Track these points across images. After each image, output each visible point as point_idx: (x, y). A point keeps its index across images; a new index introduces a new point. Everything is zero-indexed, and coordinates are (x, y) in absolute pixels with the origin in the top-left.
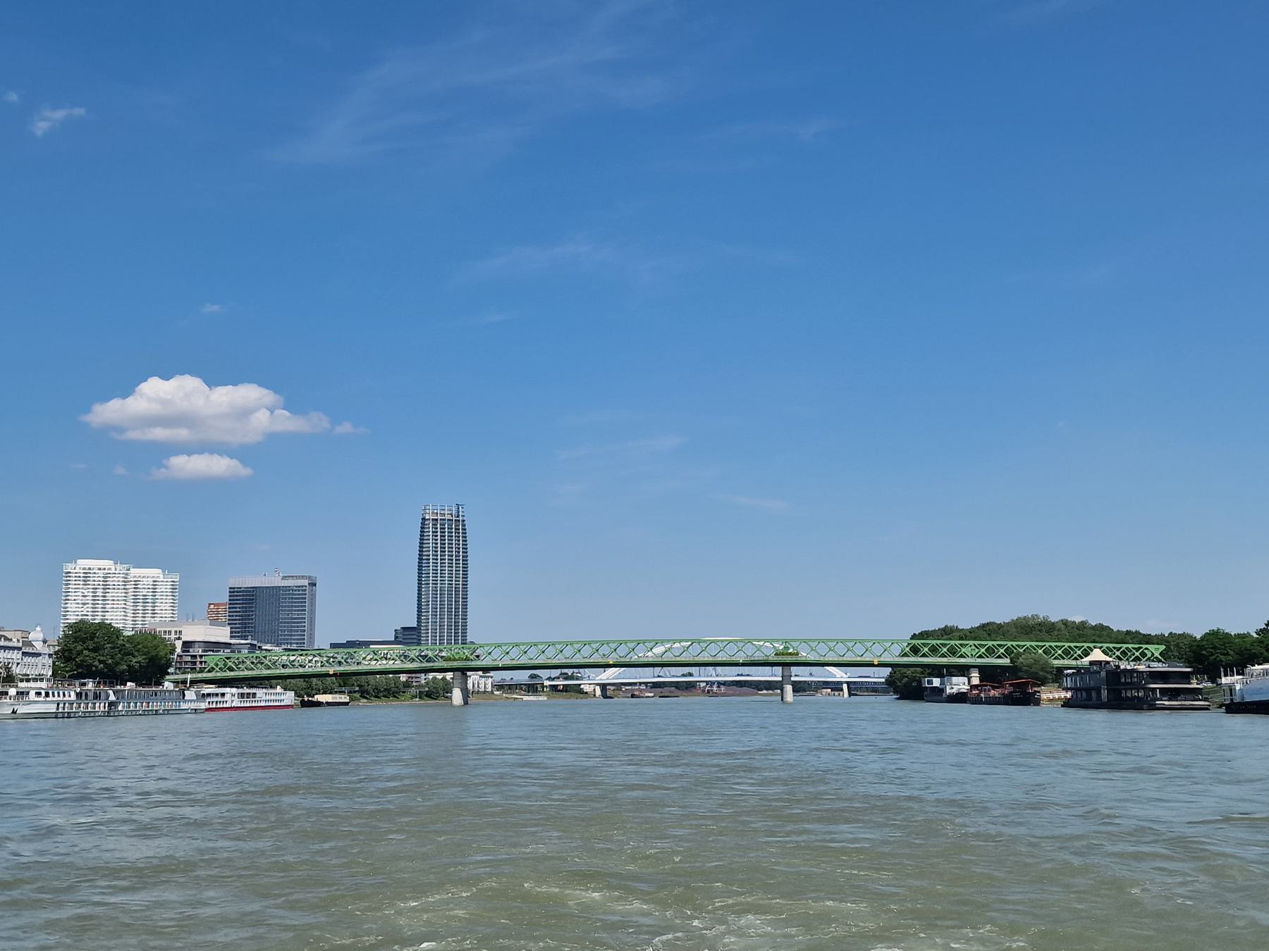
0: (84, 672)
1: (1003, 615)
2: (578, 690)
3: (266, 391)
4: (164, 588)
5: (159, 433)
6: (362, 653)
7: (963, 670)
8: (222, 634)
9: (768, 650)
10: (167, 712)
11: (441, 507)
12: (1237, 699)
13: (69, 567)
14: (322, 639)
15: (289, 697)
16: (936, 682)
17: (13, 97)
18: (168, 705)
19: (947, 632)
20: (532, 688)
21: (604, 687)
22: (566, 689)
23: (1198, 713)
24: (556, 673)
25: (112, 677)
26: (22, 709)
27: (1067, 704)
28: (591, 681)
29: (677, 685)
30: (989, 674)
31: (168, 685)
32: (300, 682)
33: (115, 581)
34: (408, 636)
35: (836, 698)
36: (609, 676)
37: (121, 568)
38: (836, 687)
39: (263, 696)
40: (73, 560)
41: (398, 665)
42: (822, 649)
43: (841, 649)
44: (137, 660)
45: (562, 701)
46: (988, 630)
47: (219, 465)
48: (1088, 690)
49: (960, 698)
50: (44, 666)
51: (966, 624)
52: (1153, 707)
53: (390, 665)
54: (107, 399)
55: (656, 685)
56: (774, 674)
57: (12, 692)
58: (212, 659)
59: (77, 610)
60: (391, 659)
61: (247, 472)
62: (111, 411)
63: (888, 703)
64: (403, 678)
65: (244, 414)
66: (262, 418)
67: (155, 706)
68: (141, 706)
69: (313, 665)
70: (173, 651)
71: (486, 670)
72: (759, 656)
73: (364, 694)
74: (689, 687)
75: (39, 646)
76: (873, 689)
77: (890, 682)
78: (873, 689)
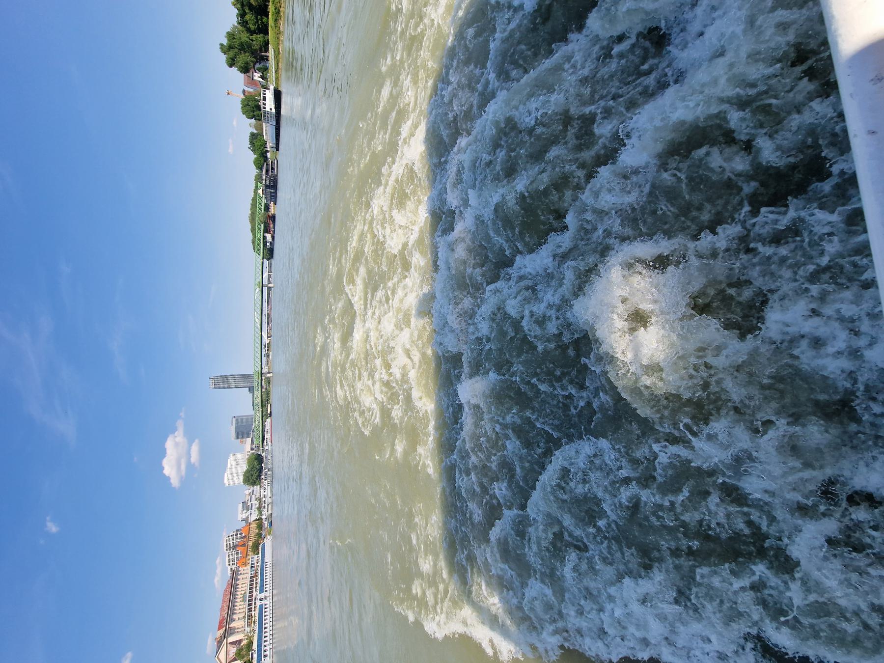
0: (259, 477)
1: (249, 226)
2: (269, 344)
3: (169, 439)
4: (234, 457)
5: (183, 467)
6: (256, 402)
7: (265, 238)
8: (249, 440)
9: (258, 290)
10: (271, 454)
11: (210, 383)
12: (275, 146)
13: (227, 485)
14: (252, 412)
15: (268, 420)
16: (268, 244)
17: (42, 542)
18: (269, 453)
19: (253, 242)
20: (268, 356)
21: (268, 337)
22: (268, 347)
23: (272, 295)
24: (263, 350)
25: (260, 470)
26: (269, 495)
27: (275, 204)
28: (266, 340)
29: (268, 318)
30: (266, 231)
31: (263, 454)
32: (264, 418)
33: (231, 471)
34: (251, 389)
35: (272, 276)
36: (265, 335)
37: (228, 471)
38: (269, 276)
39: (268, 427)
40: (224, 484)
41: (260, 392)
42: (258, 275)
43: (258, 275)
44: (256, 463)
45: (272, 347)
46: (253, 230)
47: (195, 449)
48: (271, 196)
49: (273, 237)
50: (257, 488)
51: (251, 237)
52: (277, 175)
53: (260, 394)
54: (171, 484)
55: (268, 324)
56: (265, 290)
57: (264, 499)
58: (256, 442)
59: (240, 480)
60: (258, 394)
61: (197, 441)
62: (175, 482)
63: (273, 261)
64: (263, 390)
65: (177, 444)
66: (178, 439)
67: (270, 458)
68: (270, 461)
69: (259, 414)
70: (253, 453)
71: (262, 368)
72: (260, 293)
73: (268, 400)
74: (269, 315)
75: (251, 491)
76: (270, 266)
77: (268, 259)
78: (270, 266)
